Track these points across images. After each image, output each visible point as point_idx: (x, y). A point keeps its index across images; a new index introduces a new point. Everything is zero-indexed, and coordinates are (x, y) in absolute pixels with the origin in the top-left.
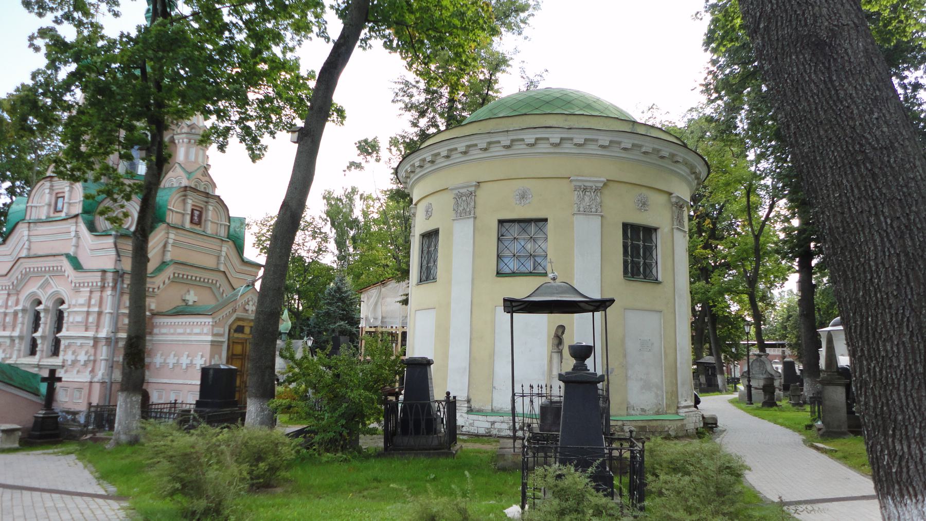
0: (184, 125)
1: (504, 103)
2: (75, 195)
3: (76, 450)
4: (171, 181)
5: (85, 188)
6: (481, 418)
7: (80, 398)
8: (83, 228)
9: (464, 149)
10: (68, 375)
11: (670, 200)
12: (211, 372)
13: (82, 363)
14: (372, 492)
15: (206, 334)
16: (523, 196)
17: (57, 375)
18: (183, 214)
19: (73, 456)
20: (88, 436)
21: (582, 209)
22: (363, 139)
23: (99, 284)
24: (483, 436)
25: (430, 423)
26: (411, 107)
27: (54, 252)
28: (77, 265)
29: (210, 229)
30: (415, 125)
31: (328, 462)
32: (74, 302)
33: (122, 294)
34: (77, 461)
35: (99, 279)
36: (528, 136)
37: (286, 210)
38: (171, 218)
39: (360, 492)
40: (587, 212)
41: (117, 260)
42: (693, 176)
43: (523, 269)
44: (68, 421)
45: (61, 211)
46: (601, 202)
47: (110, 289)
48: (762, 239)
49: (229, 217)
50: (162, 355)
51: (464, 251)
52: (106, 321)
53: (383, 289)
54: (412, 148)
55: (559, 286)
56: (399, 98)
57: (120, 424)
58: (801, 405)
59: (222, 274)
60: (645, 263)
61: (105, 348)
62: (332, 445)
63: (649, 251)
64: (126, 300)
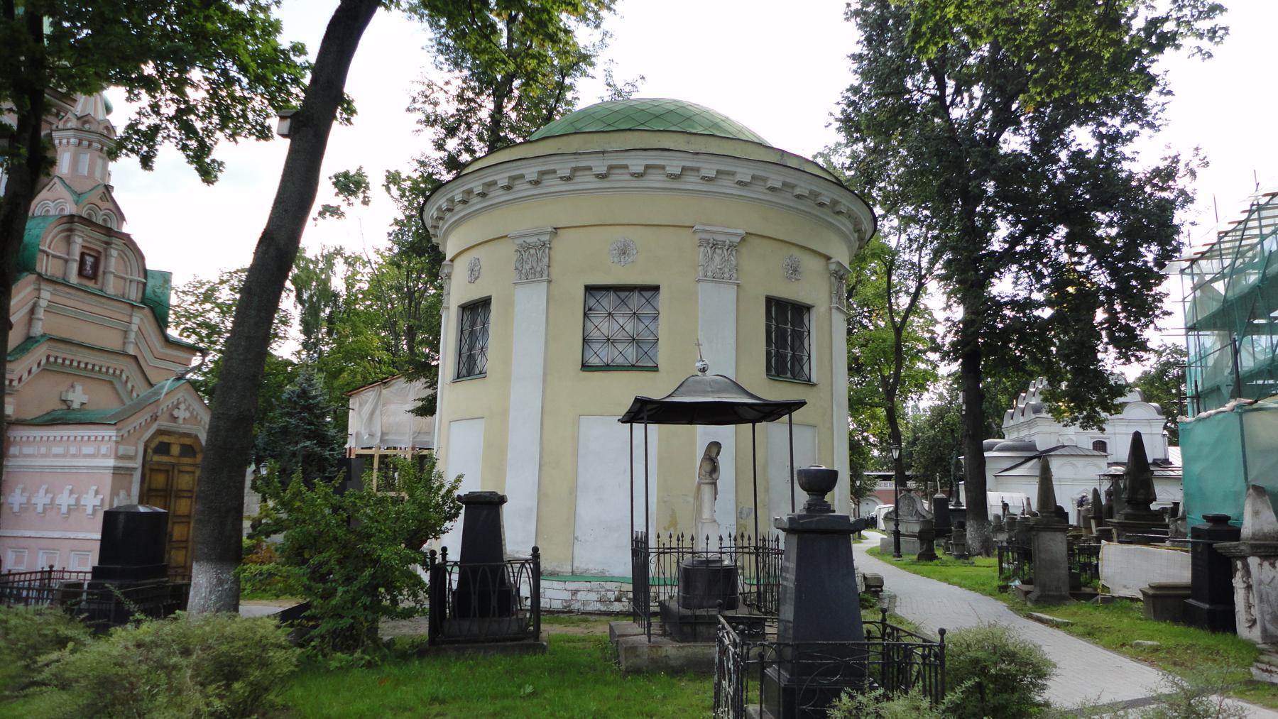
1: (588, 113)
6: (556, 585)
9: (534, 177)
11: (827, 268)
12: (122, 518)
15: (105, 456)
16: (623, 252)
18: (66, 261)
21: (710, 274)
22: (342, 170)
24: (559, 612)
25: (508, 595)
26: (435, 121)
29: (112, 286)
31: (340, 668)
36: (635, 162)
43: (620, 360)
48: (904, 334)
49: (145, 271)
50: (23, 491)
51: (529, 331)
53: (384, 392)
54: (426, 188)
56: (418, 105)
58: (967, 557)
60: (793, 356)
62: (348, 639)
63: (800, 337)
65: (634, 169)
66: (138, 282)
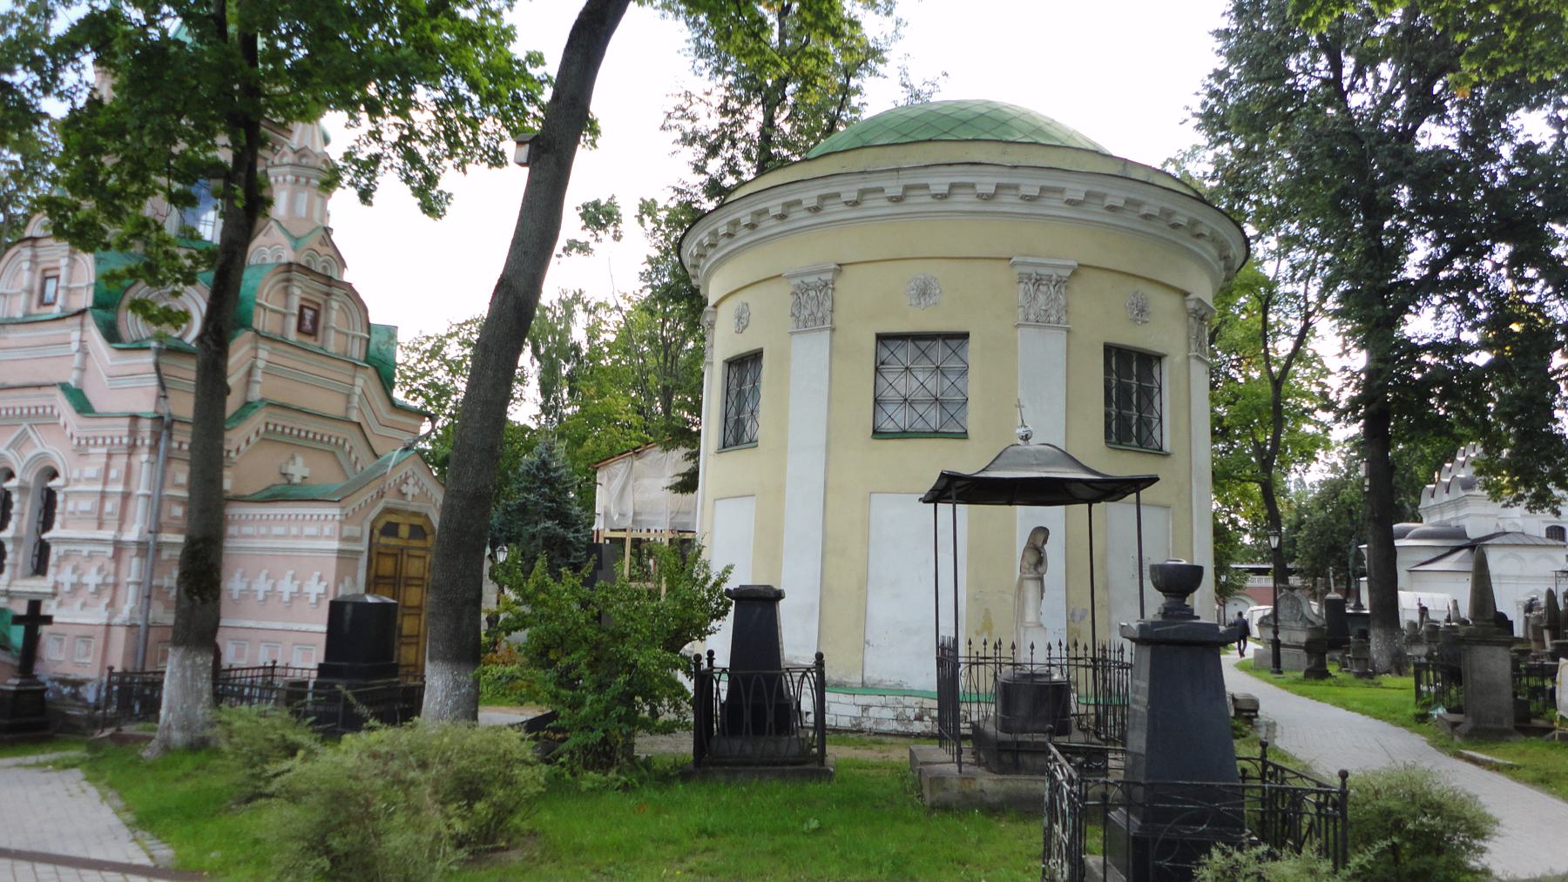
0: (286, 149)
1: (878, 122)
2: (81, 274)
3: (83, 761)
4: (263, 253)
5: (98, 261)
7: (87, 655)
8: (95, 336)
10: (63, 611)
12: (349, 609)
13: (92, 588)
14: (705, 859)
15: (328, 538)
16: (924, 291)
17: (44, 611)
18: (284, 315)
19: (77, 774)
20: (107, 732)
21: (1032, 317)
22: (591, 200)
23: (125, 440)
24: (846, 731)
25: (787, 711)
26: (694, 139)
27: (38, 380)
28: (83, 406)
29: (333, 343)
30: (700, 169)
31: (592, 790)
32: (76, 474)
33: (168, 459)
34: (85, 784)
35: (125, 431)
36: (1028, 182)
37: (507, 293)
38: (263, 321)
39: (681, 860)
40: (1041, 322)
41: (159, 397)
42: (1222, 264)
43: (919, 426)
44: (63, 697)
45: (51, 304)
46: (1067, 305)
47: (146, 450)
49: (369, 324)
50: (243, 575)
51: (810, 390)
52: (138, 509)
53: (637, 463)
54: (687, 217)
55: (1038, 451)
56: (673, 122)
57: (170, 709)
58: (1371, 676)
59: (355, 429)
61: (135, 562)
63: (1148, 395)
64: (181, 474)
65: (935, 189)
66: (361, 338)
